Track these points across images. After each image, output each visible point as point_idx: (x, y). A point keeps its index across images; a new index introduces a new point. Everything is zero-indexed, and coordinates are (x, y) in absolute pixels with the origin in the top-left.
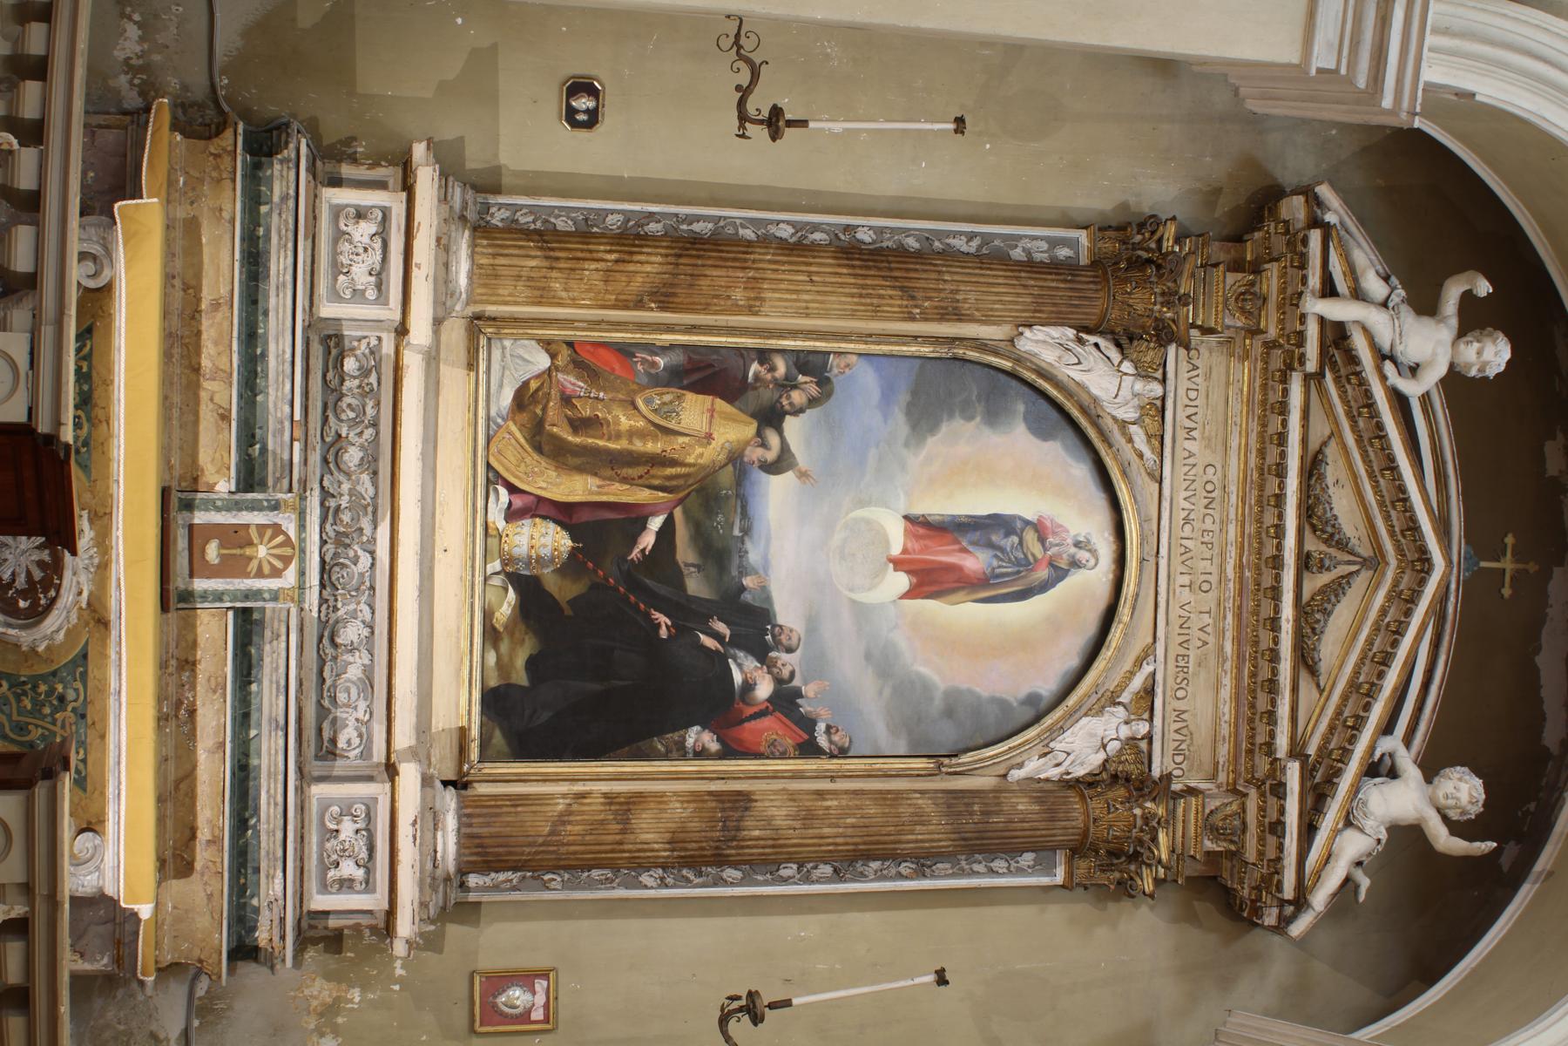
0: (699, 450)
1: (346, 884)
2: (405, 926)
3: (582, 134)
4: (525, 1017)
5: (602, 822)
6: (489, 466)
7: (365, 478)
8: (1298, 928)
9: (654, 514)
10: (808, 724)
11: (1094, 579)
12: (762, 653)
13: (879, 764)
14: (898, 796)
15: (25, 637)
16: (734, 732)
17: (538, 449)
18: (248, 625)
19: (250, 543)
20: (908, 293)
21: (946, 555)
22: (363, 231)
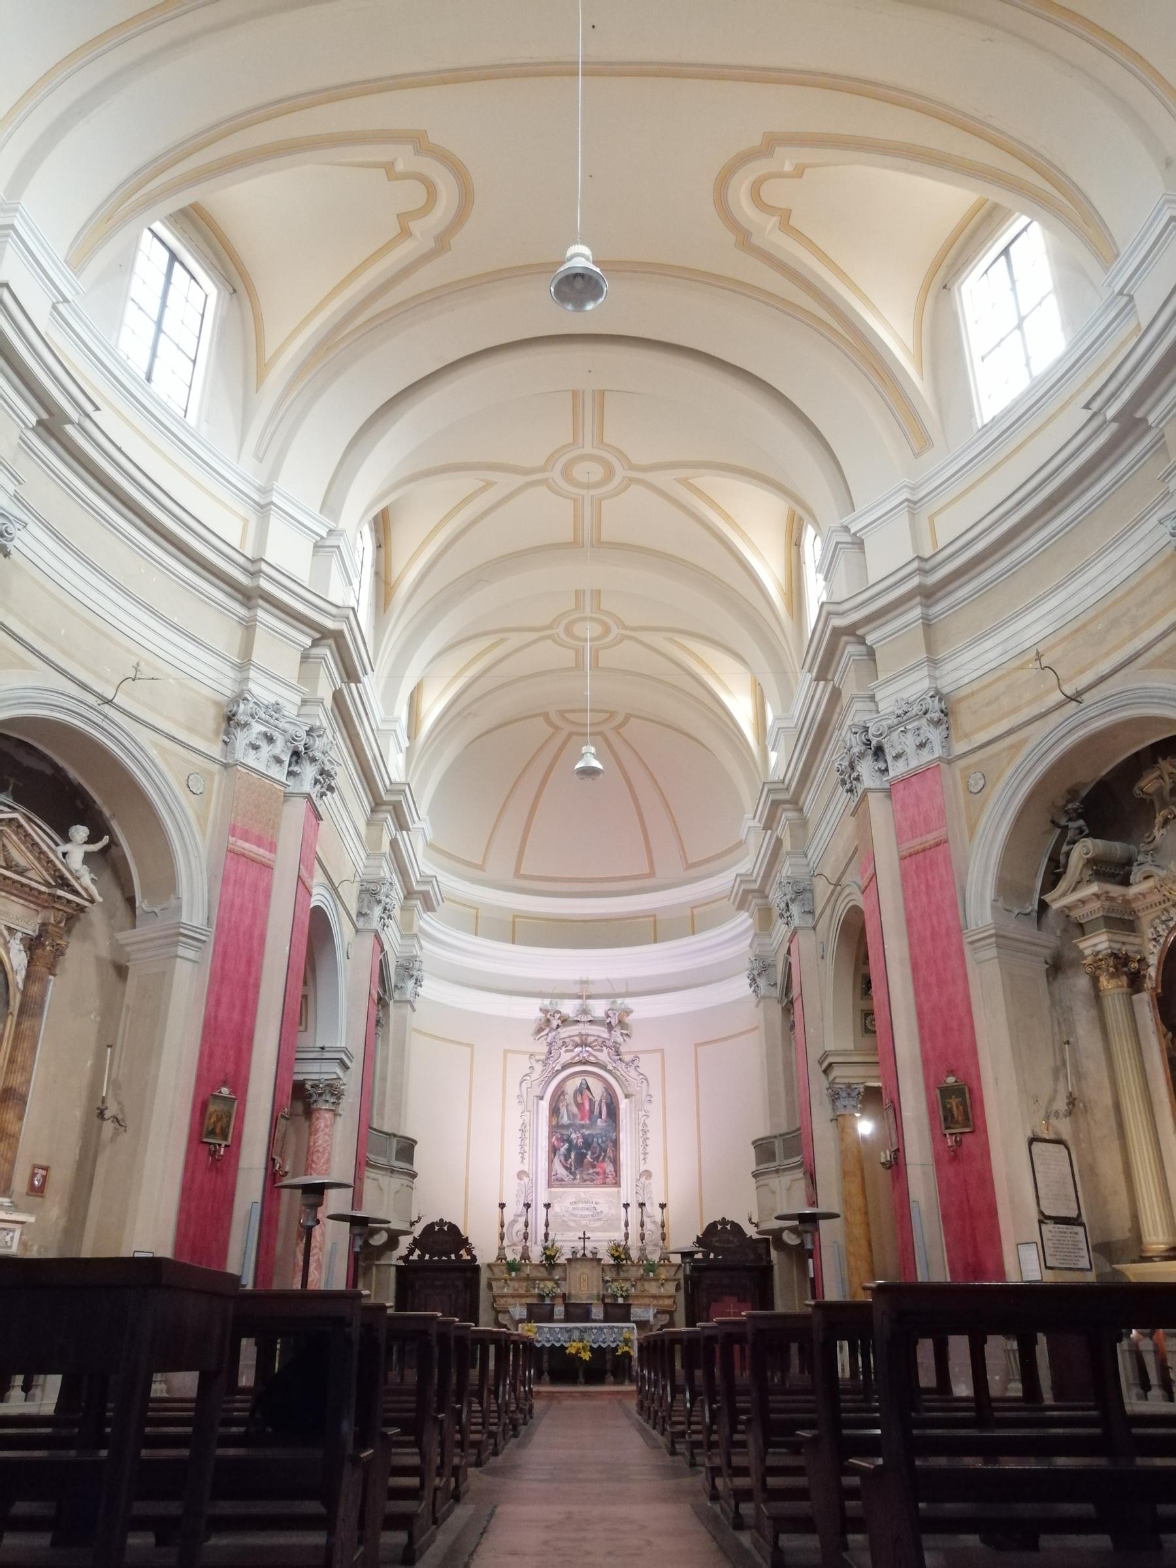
5: (9, 1144)
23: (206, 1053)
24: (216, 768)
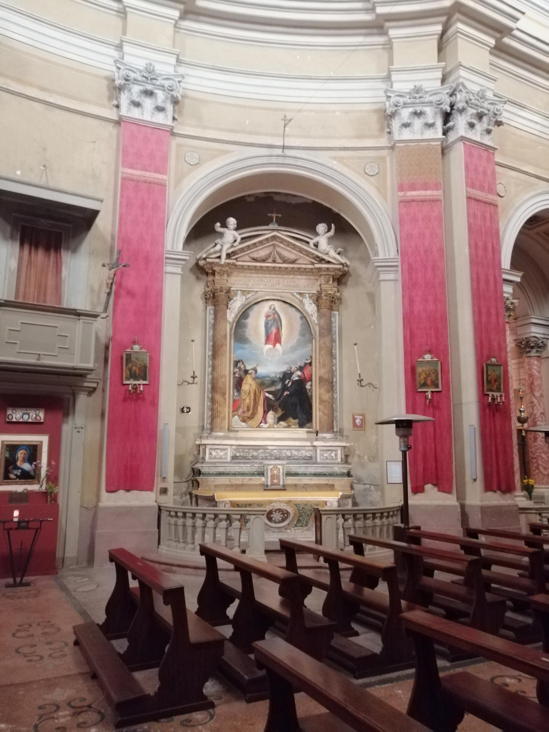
0: (253, 386)
1: (336, 455)
2: (344, 444)
3: (191, 410)
4: (362, 420)
6: (257, 427)
7: (259, 451)
8: (348, 263)
9: (265, 395)
10: (306, 364)
11: (277, 305)
12: (292, 374)
13: (314, 350)
14: (320, 347)
15: (292, 515)
16: (307, 379)
17: (253, 418)
18: (289, 474)
19: (274, 474)
20: (222, 346)
21: (273, 336)
22: (214, 453)
23: (408, 336)
24: (385, 153)
